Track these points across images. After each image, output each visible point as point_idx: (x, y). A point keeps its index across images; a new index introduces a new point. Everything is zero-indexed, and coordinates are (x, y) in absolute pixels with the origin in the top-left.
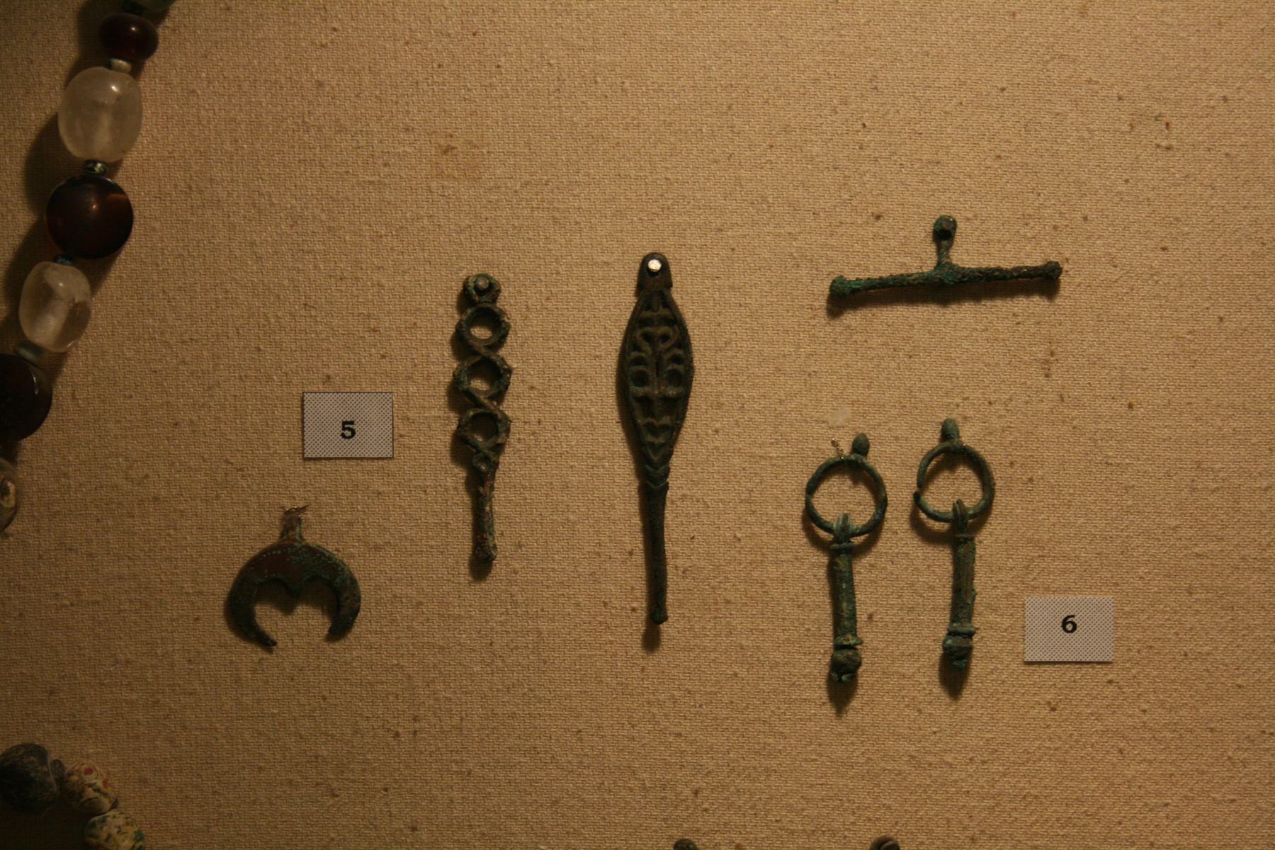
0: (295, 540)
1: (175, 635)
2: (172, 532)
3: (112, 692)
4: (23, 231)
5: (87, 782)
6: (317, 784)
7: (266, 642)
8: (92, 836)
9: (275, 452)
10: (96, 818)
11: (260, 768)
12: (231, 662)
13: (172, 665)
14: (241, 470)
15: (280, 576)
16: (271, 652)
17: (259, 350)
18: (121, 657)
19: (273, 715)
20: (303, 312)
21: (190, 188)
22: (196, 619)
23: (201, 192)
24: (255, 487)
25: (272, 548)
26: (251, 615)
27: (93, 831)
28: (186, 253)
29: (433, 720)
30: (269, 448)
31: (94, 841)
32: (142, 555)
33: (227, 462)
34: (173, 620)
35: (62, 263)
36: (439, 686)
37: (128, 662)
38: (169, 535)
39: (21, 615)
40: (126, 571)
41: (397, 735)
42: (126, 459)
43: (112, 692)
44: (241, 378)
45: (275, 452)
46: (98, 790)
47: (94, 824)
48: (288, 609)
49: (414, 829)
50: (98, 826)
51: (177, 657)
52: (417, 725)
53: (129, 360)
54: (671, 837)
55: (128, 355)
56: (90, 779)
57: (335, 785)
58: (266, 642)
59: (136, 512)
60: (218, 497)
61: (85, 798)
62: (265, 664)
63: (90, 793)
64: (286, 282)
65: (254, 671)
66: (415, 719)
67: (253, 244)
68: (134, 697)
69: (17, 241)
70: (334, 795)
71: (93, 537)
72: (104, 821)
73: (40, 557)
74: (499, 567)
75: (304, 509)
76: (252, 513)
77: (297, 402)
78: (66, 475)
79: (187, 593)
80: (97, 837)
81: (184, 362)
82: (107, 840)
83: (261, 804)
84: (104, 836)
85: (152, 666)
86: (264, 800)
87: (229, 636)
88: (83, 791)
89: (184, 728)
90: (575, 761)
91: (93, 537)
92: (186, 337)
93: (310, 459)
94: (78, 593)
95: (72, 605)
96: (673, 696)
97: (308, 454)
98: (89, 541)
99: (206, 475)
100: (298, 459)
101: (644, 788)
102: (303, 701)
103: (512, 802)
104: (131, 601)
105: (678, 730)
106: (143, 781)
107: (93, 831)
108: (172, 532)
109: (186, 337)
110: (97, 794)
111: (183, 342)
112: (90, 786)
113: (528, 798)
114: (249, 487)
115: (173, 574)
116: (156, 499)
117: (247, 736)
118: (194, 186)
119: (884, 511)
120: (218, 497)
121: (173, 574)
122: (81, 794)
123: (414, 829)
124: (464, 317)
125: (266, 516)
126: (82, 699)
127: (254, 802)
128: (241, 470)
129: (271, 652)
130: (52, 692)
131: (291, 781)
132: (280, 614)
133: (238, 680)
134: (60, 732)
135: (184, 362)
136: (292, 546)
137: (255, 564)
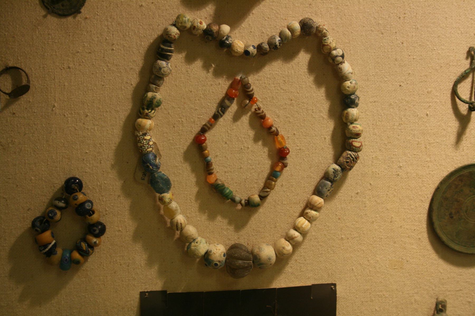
29: (409, 14)
31: (326, 44)
36: (411, 5)
41: (400, 18)
47: (325, 40)
49: (402, 43)
52: (405, 15)
54: (467, 46)
56: (325, 27)
57: (383, 31)
66: (405, 14)
70: (383, 34)
72: (328, 38)
90: (445, 26)
96: (471, 8)
101: (462, 33)
102: (376, 8)
103: (428, 36)
105: (471, 18)
113: (432, 36)
117: (361, 18)
119: (340, 77)
123: (402, 43)
124: (76, 194)
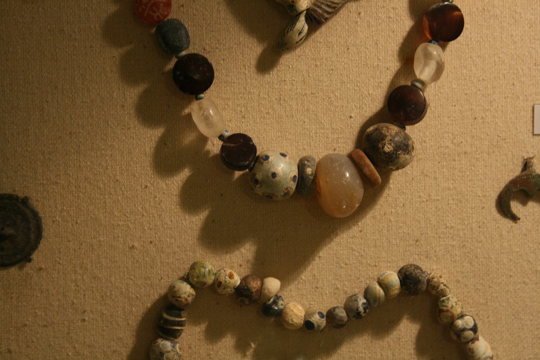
0: (532, 172)
1: (473, 215)
2: (473, 168)
3: (444, 241)
4: (408, 29)
5: (441, 282)
6: (536, 283)
7: (514, 218)
8: (443, 306)
9: (520, 132)
10: (444, 298)
11: (511, 276)
12: (498, 227)
13: (472, 229)
14: (505, 139)
15: (525, 188)
16: (516, 223)
17: (514, 84)
18: (448, 225)
19: (517, 252)
20: (534, 67)
21: (484, 9)
22: (483, 208)
23: (489, 12)
24: (511, 148)
25: (517, 177)
26: (509, 206)
27: (444, 304)
28: (481, 40)
30: (517, 130)
31: (445, 308)
32: (459, 178)
33: (498, 136)
34: (472, 208)
35: (434, 43)
37: (452, 227)
38: (471, 169)
39: (403, 205)
40: (451, 186)
42: (453, 134)
43: (444, 241)
44: (505, 98)
45: (520, 132)
46: (445, 285)
47: (443, 301)
48: (524, 203)
50: (446, 302)
51: (474, 225)
53: (454, 89)
55: (454, 86)
56: (442, 280)
58: (514, 218)
59: (456, 158)
60: (494, 152)
61: (440, 289)
62: (514, 229)
63: (442, 287)
64: (527, 54)
65: (508, 232)
67: (512, 36)
68: (454, 243)
69: (405, 34)
71: (437, 170)
72: (448, 299)
73: (413, 179)
74: (281, 156)
75: (533, 158)
76: (509, 160)
77: (531, 109)
78: (425, 142)
79: (479, 196)
80: (447, 307)
81: (480, 90)
82: (451, 308)
83: (511, 292)
84: (450, 306)
85: (463, 229)
86: (512, 290)
87: (498, 216)
88: (439, 285)
89: (477, 257)
91: (437, 170)
92: (481, 79)
93: (536, 135)
94: (430, 196)
95: (427, 201)
97: (535, 133)
98: (435, 172)
99: (489, 142)
100: (531, 135)
102: (531, 245)
104: (453, 199)
106: (458, 281)
107: (444, 304)
108: (473, 168)
109: (481, 79)
110: (445, 287)
111: (479, 81)
112: (442, 283)
114: (508, 147)
115: (472, 187)
116: (466, 153)
118: (486, 9)
120: (494, 152)
121: (472, 187)
122: (438, 287)
125: (516, 162)
126: (431, 244)
127: (508, 291)
128: (505, 139)
129: (516, 223)
130: (417, 241)
131: (524, 282)
132: (521, 206)
133: (501, 235)
134: (420, 259)
135: (480, 90)
136: (531, 175)
137: (513, 183)
